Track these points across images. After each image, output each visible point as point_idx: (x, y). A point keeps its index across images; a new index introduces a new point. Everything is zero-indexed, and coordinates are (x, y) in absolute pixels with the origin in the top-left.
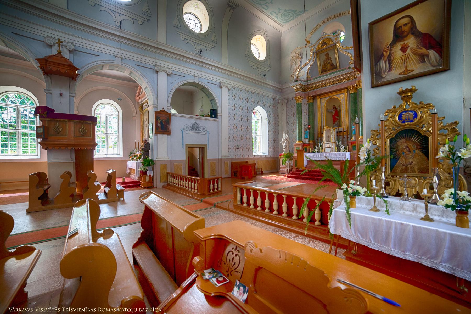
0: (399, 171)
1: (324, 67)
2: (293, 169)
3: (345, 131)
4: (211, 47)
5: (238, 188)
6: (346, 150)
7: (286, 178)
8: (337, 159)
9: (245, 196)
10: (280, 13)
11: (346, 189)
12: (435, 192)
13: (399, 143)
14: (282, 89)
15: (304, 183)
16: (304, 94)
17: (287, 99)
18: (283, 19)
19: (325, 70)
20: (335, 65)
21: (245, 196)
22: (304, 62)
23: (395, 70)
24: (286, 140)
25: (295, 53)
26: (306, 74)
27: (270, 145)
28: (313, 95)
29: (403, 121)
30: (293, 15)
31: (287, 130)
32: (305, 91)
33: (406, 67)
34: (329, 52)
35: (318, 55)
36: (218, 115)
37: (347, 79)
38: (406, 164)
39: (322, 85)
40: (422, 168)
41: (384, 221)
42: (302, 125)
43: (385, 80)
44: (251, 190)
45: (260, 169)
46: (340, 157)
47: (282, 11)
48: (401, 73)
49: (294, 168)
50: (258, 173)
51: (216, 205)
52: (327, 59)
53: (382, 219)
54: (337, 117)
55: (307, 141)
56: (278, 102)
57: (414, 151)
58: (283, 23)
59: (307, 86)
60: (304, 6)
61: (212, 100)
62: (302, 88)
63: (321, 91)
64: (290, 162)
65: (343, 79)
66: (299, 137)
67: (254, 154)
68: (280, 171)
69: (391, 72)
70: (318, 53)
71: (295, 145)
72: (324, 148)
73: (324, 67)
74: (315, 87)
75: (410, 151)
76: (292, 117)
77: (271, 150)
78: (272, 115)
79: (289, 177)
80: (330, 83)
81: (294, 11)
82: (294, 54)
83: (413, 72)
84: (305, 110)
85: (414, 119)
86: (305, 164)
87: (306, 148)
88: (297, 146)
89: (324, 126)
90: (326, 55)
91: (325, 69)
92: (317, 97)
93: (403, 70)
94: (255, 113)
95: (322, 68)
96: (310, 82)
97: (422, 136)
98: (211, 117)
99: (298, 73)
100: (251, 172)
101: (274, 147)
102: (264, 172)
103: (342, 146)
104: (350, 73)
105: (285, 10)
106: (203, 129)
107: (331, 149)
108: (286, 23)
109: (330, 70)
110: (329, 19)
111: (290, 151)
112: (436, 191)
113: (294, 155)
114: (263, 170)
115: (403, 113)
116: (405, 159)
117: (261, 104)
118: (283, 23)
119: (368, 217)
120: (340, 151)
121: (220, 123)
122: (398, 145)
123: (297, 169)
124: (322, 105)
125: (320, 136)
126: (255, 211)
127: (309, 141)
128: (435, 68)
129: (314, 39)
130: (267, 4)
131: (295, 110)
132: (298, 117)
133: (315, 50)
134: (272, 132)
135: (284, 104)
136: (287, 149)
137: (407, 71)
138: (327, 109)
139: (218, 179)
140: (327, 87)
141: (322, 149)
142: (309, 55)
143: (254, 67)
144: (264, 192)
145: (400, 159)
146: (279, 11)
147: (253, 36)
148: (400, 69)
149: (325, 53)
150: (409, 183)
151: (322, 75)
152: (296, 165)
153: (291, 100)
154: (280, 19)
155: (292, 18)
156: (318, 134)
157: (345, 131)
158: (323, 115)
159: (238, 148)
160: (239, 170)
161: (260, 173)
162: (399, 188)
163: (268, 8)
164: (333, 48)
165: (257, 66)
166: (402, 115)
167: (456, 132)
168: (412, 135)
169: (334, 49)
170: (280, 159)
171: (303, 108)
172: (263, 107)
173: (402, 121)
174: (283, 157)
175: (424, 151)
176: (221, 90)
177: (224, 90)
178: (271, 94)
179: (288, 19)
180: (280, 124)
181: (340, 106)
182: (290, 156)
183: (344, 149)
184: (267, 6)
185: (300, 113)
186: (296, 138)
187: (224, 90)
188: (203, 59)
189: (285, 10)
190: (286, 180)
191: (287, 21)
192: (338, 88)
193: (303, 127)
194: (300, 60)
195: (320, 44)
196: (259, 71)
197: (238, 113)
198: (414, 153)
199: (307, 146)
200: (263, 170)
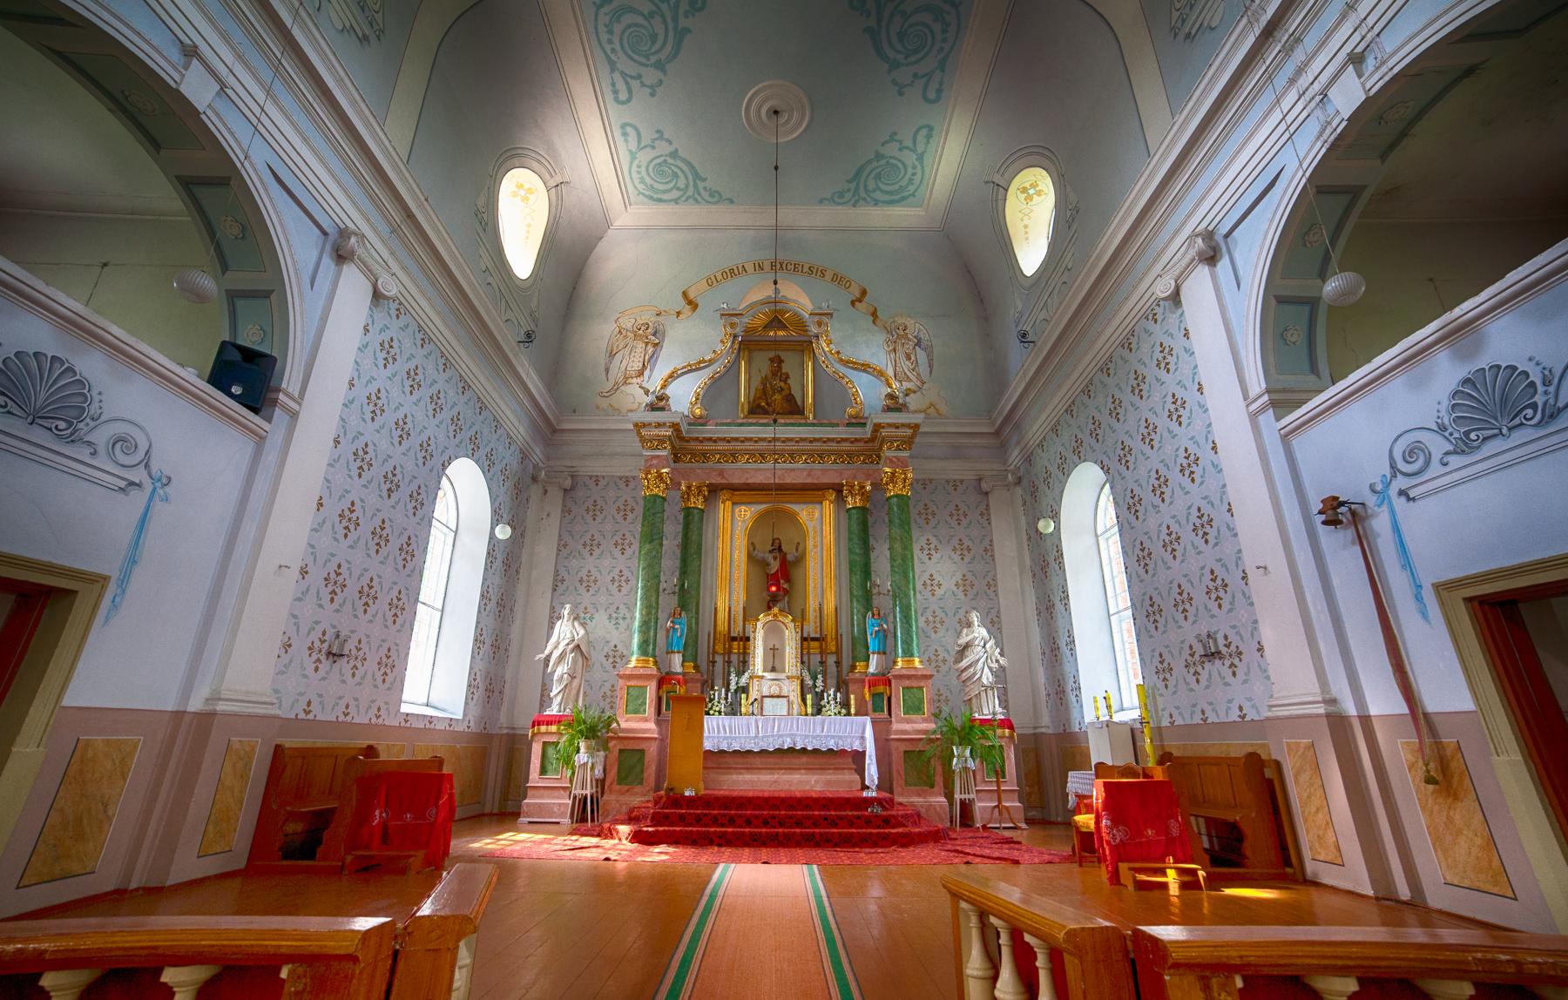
1: (760, 398)
4: (348, 25)
8: (832, 744)
10: (653, 147)
14: (554, 431)
18: (648, 180)
19: (763, 407)
20: (799, 402)
24: (572, 651)
27: (476, 670)
30: (687, 186)
34: (783, 355)
36: (275, 402)
46: (841, 738)
47: (664, 148)
58: (640, 193)
60: (776, 168)
63: (748, 476)
67: (405, 708)
68: (525, 808)
70: (747, 345)
73: (760, 398)
76: (586, 553)
81: (697, 176)
82: (627, 323)
88: (632, 683)
90: (772, 360)
91: (763, 404)
95: (751, 399)
96: (711, 430)
101: (488, 681)
105: (677, 150)
106: (120, 439)
107: (790, 703)
108: (645, 199)
117: (482, 453)
118: (640, 193)
121: (270, 458)
130: (635, 84)
135: (556, 495)
136: (574, 692)
138: (752, 546)
143: (490, 279)
146: (654, 140)
147: (517, 163)
149: (772, 354)
153: (592, 484)
154: (638, 172)
155: (675, 194)
159: (334, 656)
163: (629, 100)
172: (483, 472)
177: (352, 288)
178: (518, 427)
179: (665, 192)
184: (630, 91)
187: (352, 288)
188: (304, 26)
189: (677, 150)
191: (655, 196)
192: (809, 480)
194: (650, 350)
197: (384, 445)
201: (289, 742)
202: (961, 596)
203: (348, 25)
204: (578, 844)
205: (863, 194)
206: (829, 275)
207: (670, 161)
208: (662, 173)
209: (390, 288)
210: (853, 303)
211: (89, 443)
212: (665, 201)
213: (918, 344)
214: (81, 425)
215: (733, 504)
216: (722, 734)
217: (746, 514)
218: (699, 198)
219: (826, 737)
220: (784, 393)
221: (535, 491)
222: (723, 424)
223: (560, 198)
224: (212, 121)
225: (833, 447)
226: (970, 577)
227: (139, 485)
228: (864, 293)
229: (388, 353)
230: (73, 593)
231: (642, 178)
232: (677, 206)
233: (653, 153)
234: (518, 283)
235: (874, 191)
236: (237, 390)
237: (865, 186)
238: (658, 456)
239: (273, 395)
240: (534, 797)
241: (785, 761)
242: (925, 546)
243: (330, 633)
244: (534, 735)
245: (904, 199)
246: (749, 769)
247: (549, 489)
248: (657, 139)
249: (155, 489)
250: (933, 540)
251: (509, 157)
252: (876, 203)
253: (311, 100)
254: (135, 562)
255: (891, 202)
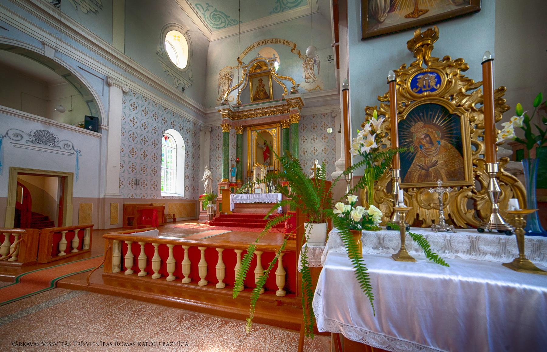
0: (416, 180)
1: (257, 95)
2: (216, 214)
3: (276, 171)
4: (88, 10)
5: (115, 241)
6: (277, 192)
7: (208, 225)
8: (268, 201)
9: (129, 256)
11: (343, 216)
12: (495, 209)
13: (413, 129)
14: (206, 114)
15: (231, 231)
16: (233, 122)
17: (211, 128)
20: (268, 94)
21: (129, 256)
22: (235, 83)
23: (400, 9)
24: (208, 178)
25: (224, 73)
26: (236, 99)
28: (243, 125)
29: (419, 89)
30: (225, 20)
31: (210, 166)
32: (233, 119)
33: (416, 4)
35: (251, 79)
36: (101, 128)
37: (280, 111)
38: (426, 165)
39: (254, 115)
40: (452, 172)
41: (456, 284)
42: (228, 160)
43: (384, 27)
44: (140, 243)
45: (172, 215)
46: (271, 199)
47: (212, 9)
48: (409, 15)
49: (218, 214)
50: (168, 220)
51: (57, 283)
52: (260, 86)
53: (451, 280)
54: (268, 154)
55: (234, 180)
56: (200, 130)
57: (439, 142)
59: (237, 113)
60: (239, 10)
61: (91, 101)
62: (230, 114)
64: (213, 205)
65: (276, 112)
66: (225, 175)
67: (163, 195)
68: (200, 217)
69: (394, 13)
70: (251, 76)
71: (219, 184)
72: (253, 189)
73: (257, 95)
74: (245, 115)
75: (431, 143)
77: (188, 191)
78: (191, 144)
79: (211, 224)
80: (262, 113)
81: (227, 17)
83: (428, 13)
84: (233, 144)
85: (436, 85)
86: (232, 207)
87: (232, 189)
89: (253, 163)
92: (248, 129)
93: (411, 10)
94: (166, 138)
95: (254, 95)
96: (241, 109)
97: (450, 115)
98: (86, 127)
99: (227, 96)
100: (157, 218)
102: (177, 220)
103: (273, 186)
104: (284, 105)
107: (262, 190)
108: (216, 29)
109: (262, 99)
110: (264, 42)
111: (213, 192)
112: (497, 207)
113: (218, 197)
114: (175, 217)
115: (419, 77)
116: (425, 157)
117: (177, 126)
118: (212, 27)
119: (414, 277)
120: (271, 193)
121: (104, 141)
122: (413, 133)
123: (222, 214)
124: (252, 138)
125: (249, 175)
126: (146, 282)
127: (236, 180)
128: (459, 7)
129: (246, 60)
131: (221, 141)
132: (224, 149)
133: (247, 72)
134: (190, 167)
135: (208, 134)
136: (210, 189)
137: (417, 11)
138: (257, 144)
139: (82, 230)
140: (259, 117)
141: (252, 189)
142: (239, 76)
143: (168, 73)
144: (166, 245)
145: (416, 157)
147: (168, 29)
148: (408, 7)
149: (259, 78)
150: (430, 199)
151: (254, 103)
152: (220, 209)
153: (217, 129)
154: (209, 20)
155: (223, 25)
156: (247, 172)
157: (276, 171)
158: (253, 151)
159: (137, 184)
160: (137, 215)
161: (172, 220)
162: (417, 210)
164: (267, 74)
165: (174, 74)
166: (417, 79)
167: (502, 106)
168: (433, 114)
169: (268, 75)
170: (199, 202)
171: (230, 141)
172: (179, 132)
173: (417, 91)
174: (203, 199)
175: (456, 142)
176: (110, 89)
177: (116, 95)
178: (191, 117)
180: (201, 158)
181: (271, 142)
182: (212, 198)
183: (275, 190)
185: (226, 145)
186: (221, 176)
190: (207, 228)
191: (218, 27)
192: (271, 121)
193: (230, 162)
194: (230, 82)
195: (254, 66)
196: (176, 82)
198: (439, 146)
199: (233, 185)
200: (175, 217)
201: (126, 203)
202: (324, 154)
203: (88, 10)
204: (195, 225)
205: (284, 6)
206: (282, 41)
207: (216, 13)
208: (215, 18)
209: (127, 90)
210: (292, 51)
211: (59, 147)
212: (221, 28)
213: (314, 63)
214: (55, 143)
215: (251, 131)
216: (241, 199)
217: (255, 135)
218: (231, 24)
219: (267, 199)
220: (264, 92)
221: (202, 134)
222: (246, 106)
223: (189, 36)
224: (58, 61)
225: (278, 108)
226: (327, 147)
227: (73, 153)
228: (295, 46)
229: (134, 107)
230: (67, 177)
231: (210, 22)
232: (226, 29)
233: (210, 12)
234: (180, 70)
235: (287, 3)
236: (90, 127)
237: (283, 3)
238: (225, 120)
239: (100, 127)
240: (202, 215)
241: (258, 206)
242: (313, 138)
243: (134, 180)
244: (200, 200)
245: (300, 3)
246: (249, 208)
247: (206, 132)
248: (208, 7)
249: (77, 154)
250: (316, 136)
251: (165, 29)
252: (290, 8)
253: (83, 42)
254: (78, 169)
255: (296, 6)
